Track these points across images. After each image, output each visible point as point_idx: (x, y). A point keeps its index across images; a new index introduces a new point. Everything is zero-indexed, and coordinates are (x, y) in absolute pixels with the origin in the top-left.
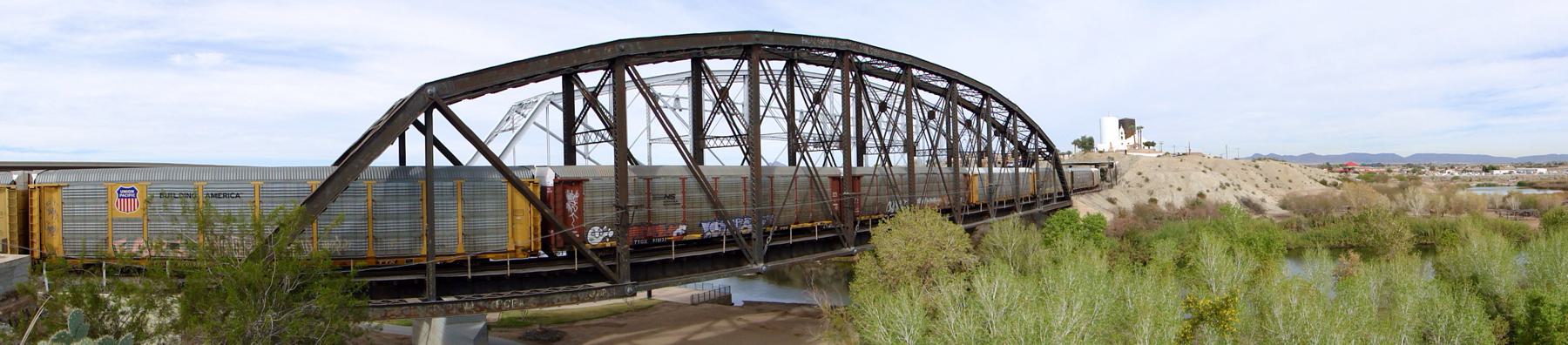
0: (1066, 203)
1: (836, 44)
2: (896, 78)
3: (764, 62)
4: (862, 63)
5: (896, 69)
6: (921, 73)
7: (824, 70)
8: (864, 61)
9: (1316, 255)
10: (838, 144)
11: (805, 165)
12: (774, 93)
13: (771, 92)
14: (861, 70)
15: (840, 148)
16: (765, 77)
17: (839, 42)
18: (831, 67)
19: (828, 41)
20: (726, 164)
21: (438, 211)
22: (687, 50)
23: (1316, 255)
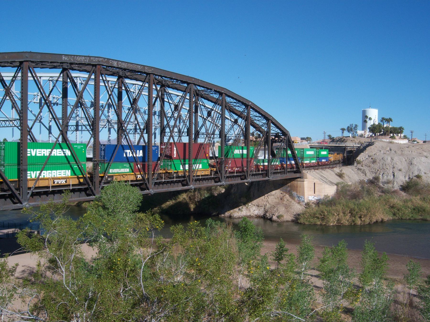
0: (298, 175)
1: (117, 64)
2: (216, 102)
3: (103, 76)
4: (199, 91)
5: (216, 96)
6: (232, 100)
7: (180, 94)
8: (200, 89)
9: (134, 212)
10: (186, 134)
11: (173, 142)
12: (110, 98)
13: (168, 103)
14: (198, 94)
15: (147, 133)
16: (32, 79)
17: (92, 58)
18: (184, 91)
19: (83, 58)
20: (100, 133)
21: (88, 142)
22: (51, 62)
23: (134, 212)
